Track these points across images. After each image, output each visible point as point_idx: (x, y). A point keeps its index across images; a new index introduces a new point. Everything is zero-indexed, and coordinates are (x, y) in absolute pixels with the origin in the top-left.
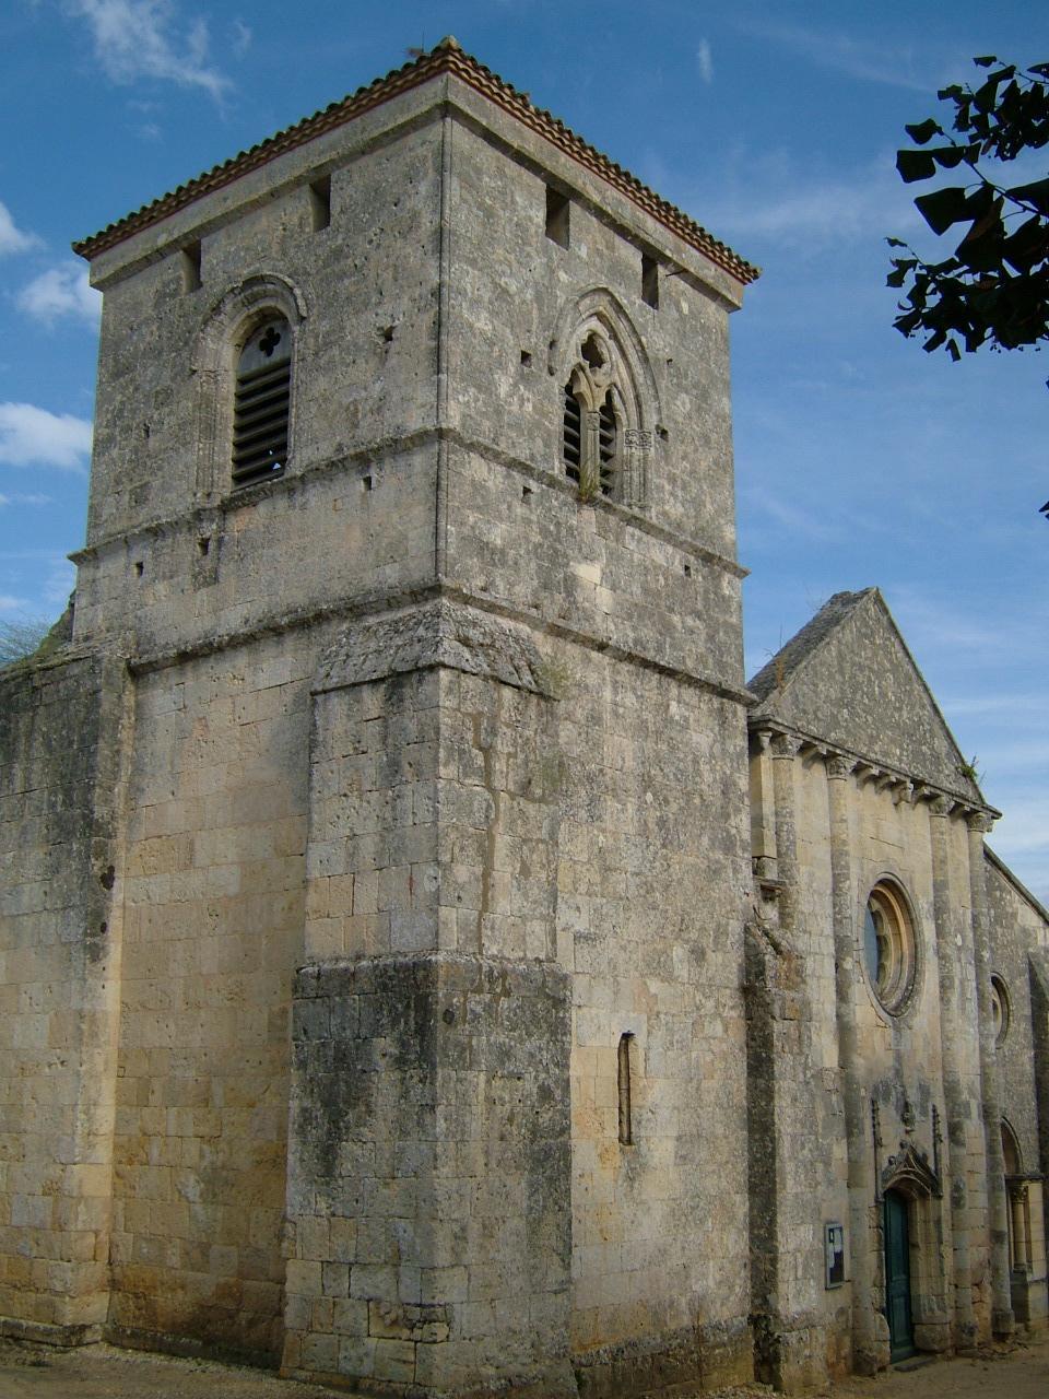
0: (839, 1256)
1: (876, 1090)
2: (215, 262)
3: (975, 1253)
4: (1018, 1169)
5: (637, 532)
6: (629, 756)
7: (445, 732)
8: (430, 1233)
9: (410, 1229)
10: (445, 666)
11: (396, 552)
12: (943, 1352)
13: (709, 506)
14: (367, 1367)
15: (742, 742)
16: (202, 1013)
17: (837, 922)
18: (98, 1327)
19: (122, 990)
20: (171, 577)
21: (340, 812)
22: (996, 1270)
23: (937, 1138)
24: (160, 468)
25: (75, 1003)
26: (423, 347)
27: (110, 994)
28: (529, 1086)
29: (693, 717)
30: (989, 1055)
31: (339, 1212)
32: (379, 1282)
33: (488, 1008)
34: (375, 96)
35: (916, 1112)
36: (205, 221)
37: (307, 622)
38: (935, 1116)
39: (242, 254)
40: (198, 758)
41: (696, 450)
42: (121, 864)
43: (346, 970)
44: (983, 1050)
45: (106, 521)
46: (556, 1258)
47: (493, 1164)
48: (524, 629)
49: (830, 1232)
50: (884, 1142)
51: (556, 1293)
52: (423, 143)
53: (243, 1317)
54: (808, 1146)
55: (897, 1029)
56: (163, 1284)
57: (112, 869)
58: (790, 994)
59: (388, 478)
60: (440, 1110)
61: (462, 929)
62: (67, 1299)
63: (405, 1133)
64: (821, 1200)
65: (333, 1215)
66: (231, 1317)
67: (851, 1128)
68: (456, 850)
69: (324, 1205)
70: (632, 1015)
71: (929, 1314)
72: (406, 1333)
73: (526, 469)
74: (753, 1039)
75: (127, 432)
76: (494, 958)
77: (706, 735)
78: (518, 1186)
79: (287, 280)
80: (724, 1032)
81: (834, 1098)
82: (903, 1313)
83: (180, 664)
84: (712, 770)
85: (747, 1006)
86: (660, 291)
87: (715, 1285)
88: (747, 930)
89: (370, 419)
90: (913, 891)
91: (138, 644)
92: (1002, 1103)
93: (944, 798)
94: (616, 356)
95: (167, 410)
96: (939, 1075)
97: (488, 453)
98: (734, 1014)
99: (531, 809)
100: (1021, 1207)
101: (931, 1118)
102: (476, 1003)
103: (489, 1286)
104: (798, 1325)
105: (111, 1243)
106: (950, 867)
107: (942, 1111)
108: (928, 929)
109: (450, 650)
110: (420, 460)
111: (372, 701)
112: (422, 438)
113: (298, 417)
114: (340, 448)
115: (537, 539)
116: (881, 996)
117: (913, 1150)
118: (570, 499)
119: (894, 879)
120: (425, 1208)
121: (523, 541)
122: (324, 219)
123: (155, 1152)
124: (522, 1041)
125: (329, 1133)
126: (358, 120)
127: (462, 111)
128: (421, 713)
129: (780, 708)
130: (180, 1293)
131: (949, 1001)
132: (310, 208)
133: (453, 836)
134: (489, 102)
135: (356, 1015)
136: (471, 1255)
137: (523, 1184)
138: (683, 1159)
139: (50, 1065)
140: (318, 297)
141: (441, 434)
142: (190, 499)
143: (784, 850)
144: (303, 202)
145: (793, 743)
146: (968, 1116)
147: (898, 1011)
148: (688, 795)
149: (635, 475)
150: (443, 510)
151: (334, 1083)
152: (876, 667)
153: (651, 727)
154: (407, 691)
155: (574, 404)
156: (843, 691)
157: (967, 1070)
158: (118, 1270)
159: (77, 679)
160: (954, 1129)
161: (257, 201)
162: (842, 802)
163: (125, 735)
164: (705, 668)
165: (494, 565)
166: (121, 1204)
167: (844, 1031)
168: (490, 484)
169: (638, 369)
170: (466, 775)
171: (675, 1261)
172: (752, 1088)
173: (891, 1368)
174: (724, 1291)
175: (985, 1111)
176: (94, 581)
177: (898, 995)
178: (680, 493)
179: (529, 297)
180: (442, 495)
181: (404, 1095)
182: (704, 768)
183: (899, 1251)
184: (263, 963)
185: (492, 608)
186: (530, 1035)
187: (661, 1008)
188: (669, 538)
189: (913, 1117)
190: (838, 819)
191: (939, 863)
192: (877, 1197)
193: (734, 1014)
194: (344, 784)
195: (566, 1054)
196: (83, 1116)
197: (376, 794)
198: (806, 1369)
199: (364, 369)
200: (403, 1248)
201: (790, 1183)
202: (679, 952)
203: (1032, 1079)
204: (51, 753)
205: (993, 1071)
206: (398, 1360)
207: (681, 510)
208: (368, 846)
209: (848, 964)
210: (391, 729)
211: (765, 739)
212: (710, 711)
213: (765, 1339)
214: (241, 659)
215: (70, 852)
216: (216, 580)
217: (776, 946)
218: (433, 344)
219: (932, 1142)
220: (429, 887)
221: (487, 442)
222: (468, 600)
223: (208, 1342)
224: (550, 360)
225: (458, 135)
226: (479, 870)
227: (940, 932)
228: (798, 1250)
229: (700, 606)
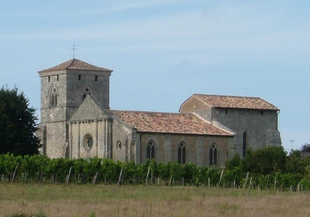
202: (58, 150)
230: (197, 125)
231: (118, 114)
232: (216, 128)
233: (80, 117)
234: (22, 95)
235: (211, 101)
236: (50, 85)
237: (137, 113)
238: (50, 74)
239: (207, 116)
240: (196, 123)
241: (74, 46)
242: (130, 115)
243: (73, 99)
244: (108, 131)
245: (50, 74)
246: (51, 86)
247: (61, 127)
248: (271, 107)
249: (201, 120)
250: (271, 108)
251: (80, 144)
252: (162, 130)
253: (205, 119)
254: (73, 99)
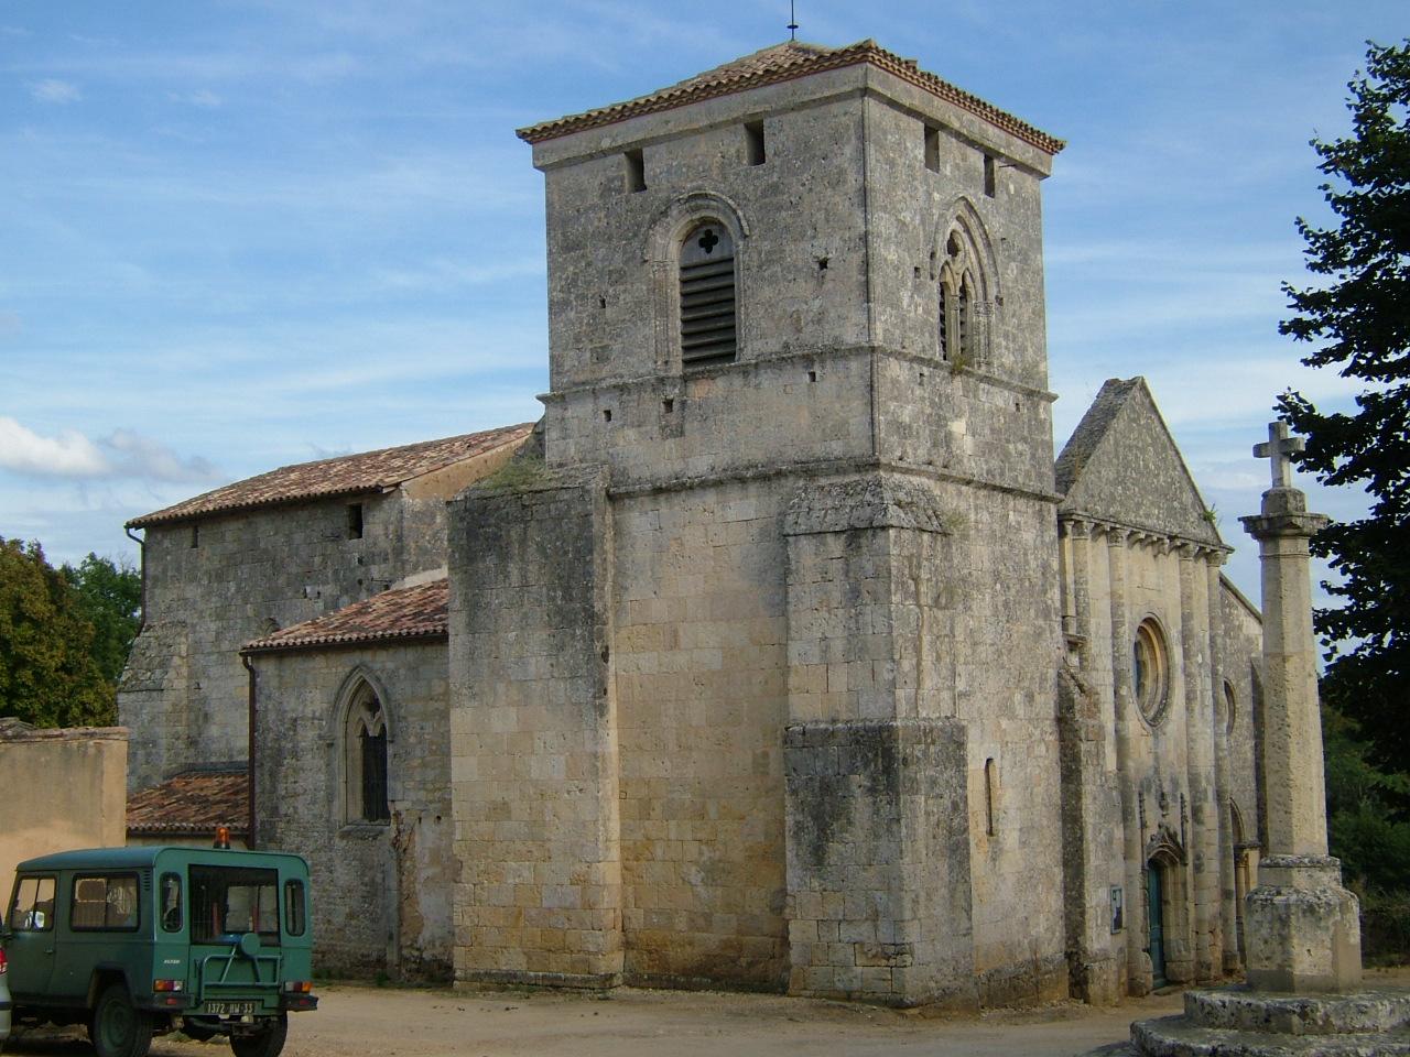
0: (1119, 912)
1: (1142, 786)
2: (658, 171)
3: (1211, 908)
4: (1240, 840)
5: (986, 386)
6: (985, 558)
7: (894, 572)
8: (900, 899)
9: (884, 897)
10: (892, 527)
11: (840, 431)
12: (1187, 982)
13: (1030, 349)
14: (856, 985)
15: (1054, 533)
16: (694, 754)
17: (1115, 659)
18: (619, 975)
19: (619, 737)
20: (639, 426)
21: (813, 621)
22: (1226, 920)
23: (1184, 818)
24: (619, 335)
25: (589, 747)
26: (854, 279)
27: (612, 741)
28: (947, 802)
29: (1020, 513)
30: (1222, 750)
31: (830, 888)
32: (863, 931)
33: (925, 753)
34: (805, 70)
35: (1169, 799)
36: (648, 136)
37: (768, 476)
38: (1183, 802)
39: (684, 170)
40: (680, 576)
41: (1021, 307)
42: (612, 644)
43: (827, 730)
44: (1217, 746)
45: (568, 371)
46: (964, 914)
47: (930, 854)
48: (924, 480)
49: (1114, 892)
50: (1148, 824)
51: (965, 935)
52: (846, 114)
53: (743, 961)
54: (1104, 831)
55: (1156, 737)
56: (672, 942)
57: (607, 648)
58: (1091, 722)
59: (830, 376)
60: (902, 821)
61: (907, 703)
62: (600, 956)
63: (877, 837)
64: (1112, 874)
65: (825, 890)
66: (733, 962)
67: (1126, 816)
68: (903, 650)
69: (817, 884)
70: (992, 745)
71: (1177, 954)
72: (884, 962)
73: (921, 361)
74: (1065, 756)
75: (582, 300)
76: (924, 719)
77: (1029, 527)
78: (944, 868)
79: (730, 201)
80: (1046, 753)
81: (1114, 793)
82: (1158, 954)
83: (654, 495)
84: (1036, 559)
85: (1061, 731)
86: (996, 181)
87: (1045, 932)
88: (1059, 675)
89: (810, 328)
90: (1167, 624)
91: (612, 476)
92: (1231, 786)
93: (1192, 546)
94: (968, 246)
95: (622, 288)
96: (1185, 769)
97: (899, 356)
98: (1052, 738)
99: (940, 614)
100: (1242, 871)
101: (1179, 804)
102: (918, 750)
103: (930, 931)
104: (1099, 958)
105: (623, 916)
106: (1194, 603)
107: (1187, 798)
108: (1177, 653)
109: (895, 515)
110: (855, 365)
111: (836, 546)
112: (858, 351)
113: (747, 315)
114: (786, 346)
115: (928, 411)
116: (1143, 710)
117: (1167, 829)
118: (947, 374)
119: (1153, 617)
120: (895, 884)
121: (920, 415)
122: (759, 157)
123: (659, 852)
124: (942, 773)
125: (819, 837)
126: (788, 84)
127: (875, 91)
128: (876, 558)
129: (1077, 499)
130: (688, 948)
131: (1192, 710)
132: (745, 143)
133: (900, 641)
134: (891, 76)
135: (836, 760)
136: (922, 913)
137: (946, 866)
138: (1023, 844)
139: (569, 792)
140: (758, 221)
141: (873, 349)
142: (651, 365)
143: (1081, 610)
144: (739, 138)
145: (1088, 526)
146: (1206, 799)
147: (1155, 721)
148: (1021, 580)
149: (982, 337)
150: (876, 406)
151: (821, 804)
152: (1140, 445)
153: (999, 535)
154: (863, 541)
155: (943, 288)
156: (1118, 472)
157: (1205, 764)
158: (631, 935)
159: (568, 504)
160: (1196, 811)
161: (697, 129)
162: (1119, 564)
163: (609, 546)
164: (1030, 481)
165: (906, 438)
166: (630, 889)
167: (1121, 742)
168: (901, 378)
169: (983, 254)
170: (906, 599)
171: (1021, 915)
172: (1065, 791)
173: (1152, 993)
174: (1049, 935)
175: (1218, 796)
176: (563, 419)
177: (1155, 707)
178: (1011, 345)
179: (917, 222)
180: (875, 394)
181: (877, 812)
182: (1031, 557)
183: (1157, 906)
184: (746, 719)
185: (907, 471)
186: (946, 768)
187: (1008, 739)
188: (1007, 386)
189: (1168, 804)
190: (1116, 577)
191: (1186, 598)
192: (1143, 867)
193: (1052, 738)
194: (815, 601)
195: (965, 778)
196: (602, 828)
197: (842, 611)
198: (1105, 989)
199: (804, 287)
200: (880, 909)
201: (1092, 858)
202: (1018, 697)
203: (1253, 764)
204: (546, 558)
205: (1226, 764)
206: (880, 979)
207: (1012, 358)
208: (838, 646)
209: (1124, 691)
210: (852, 567)
211: (1069, 527)
212: (1034, 513)
213: (1077, 968)
214: (711, 497)
215: (573, 636)
216: (682, 433)
217: (1080, 687)
218: (864, 279)
219: (1179, 822)
220: (888, 676)
221: (898, 348)
222: (893, 469)
223: (716, 979)
224: (931, 268)
225: (874, 109)
226: (914, 661)
227: (1186, 655)
228: (1098, 906)
229: (1026, 433)
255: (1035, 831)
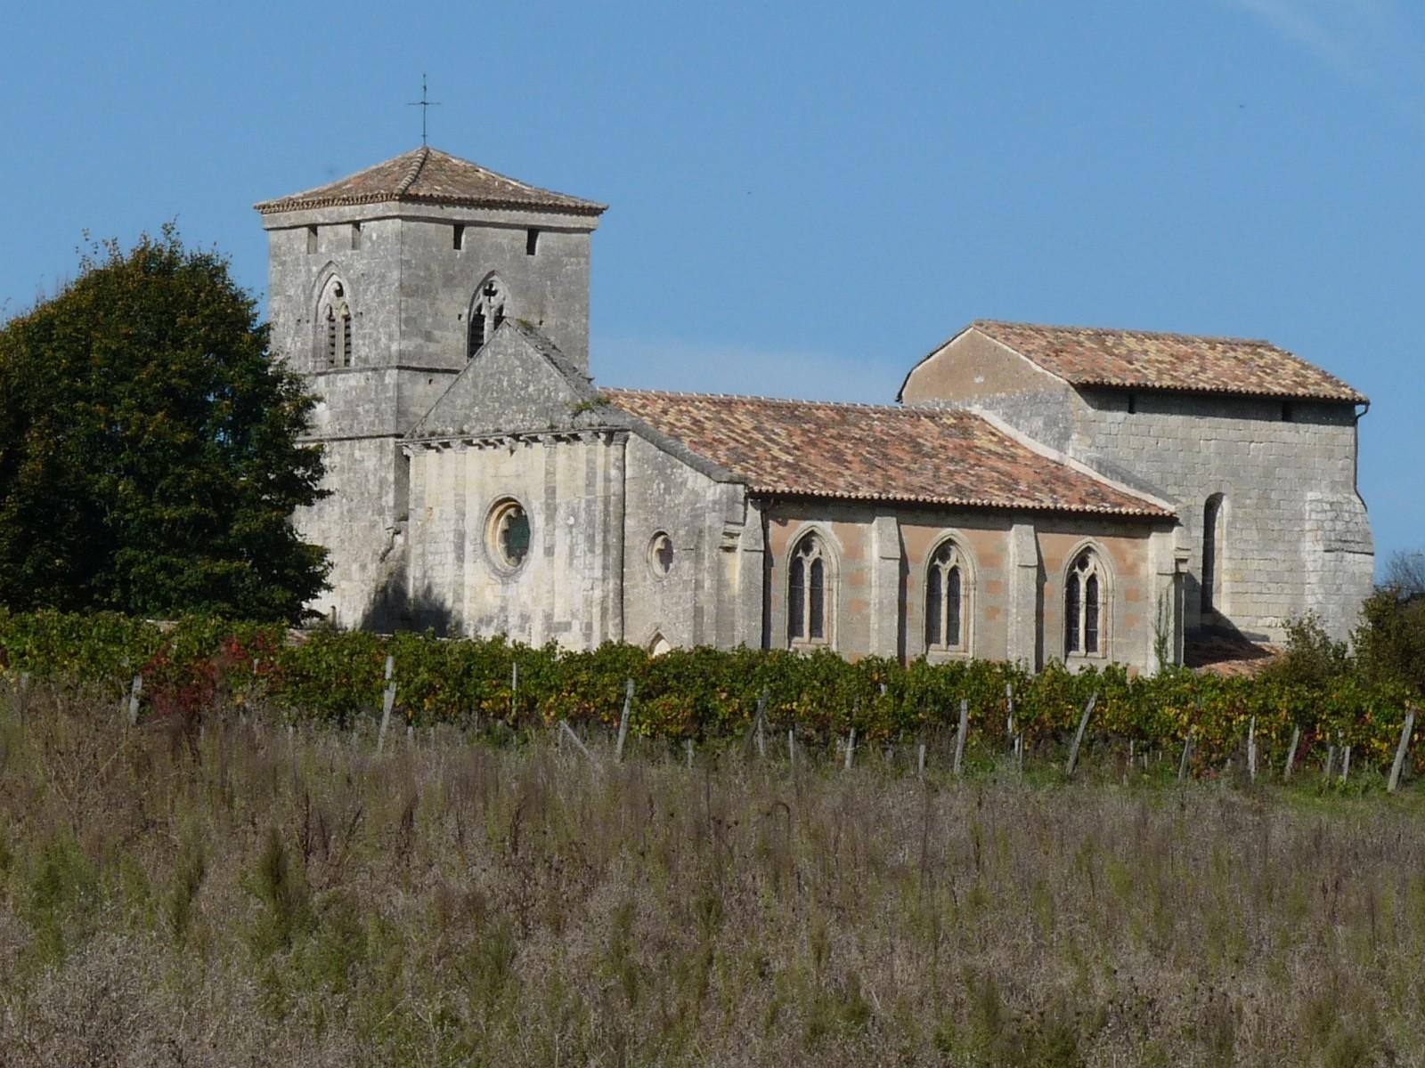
148: (362, 494)
202: (355, 567)
230: (1000, 465)
231: (644, 406)
232: (1091, 479)
233: (468, 417)
234: (1299, 632)
235: (1057, 352)
236: (315, 269)
237: (728, 404)
238: (315, 215)
239: (1040, 423)
240: (996, 453)
241: (425, 88)
242: (695, 411)
243: (428, 337)
244: (606, 489)
245: (315, 215)
246: (323, 270)
247: (371, 463)
248: (1327, 386)
249: (1011, 439)
250: (1327, 390)
251: (467, 544)
252: (856, 488)
253: (1033, 435)
254: (428, 337)
255: (318, 983)
